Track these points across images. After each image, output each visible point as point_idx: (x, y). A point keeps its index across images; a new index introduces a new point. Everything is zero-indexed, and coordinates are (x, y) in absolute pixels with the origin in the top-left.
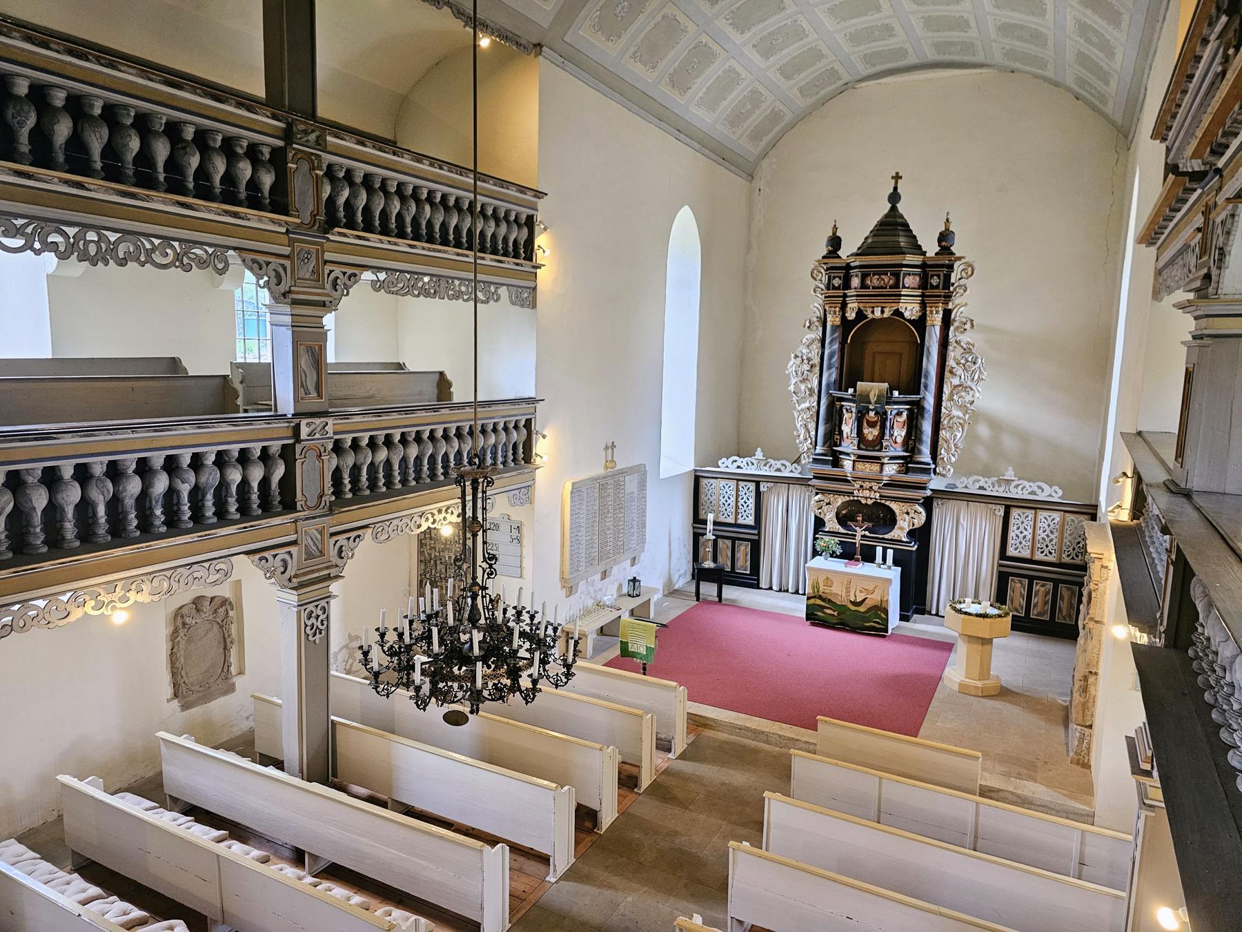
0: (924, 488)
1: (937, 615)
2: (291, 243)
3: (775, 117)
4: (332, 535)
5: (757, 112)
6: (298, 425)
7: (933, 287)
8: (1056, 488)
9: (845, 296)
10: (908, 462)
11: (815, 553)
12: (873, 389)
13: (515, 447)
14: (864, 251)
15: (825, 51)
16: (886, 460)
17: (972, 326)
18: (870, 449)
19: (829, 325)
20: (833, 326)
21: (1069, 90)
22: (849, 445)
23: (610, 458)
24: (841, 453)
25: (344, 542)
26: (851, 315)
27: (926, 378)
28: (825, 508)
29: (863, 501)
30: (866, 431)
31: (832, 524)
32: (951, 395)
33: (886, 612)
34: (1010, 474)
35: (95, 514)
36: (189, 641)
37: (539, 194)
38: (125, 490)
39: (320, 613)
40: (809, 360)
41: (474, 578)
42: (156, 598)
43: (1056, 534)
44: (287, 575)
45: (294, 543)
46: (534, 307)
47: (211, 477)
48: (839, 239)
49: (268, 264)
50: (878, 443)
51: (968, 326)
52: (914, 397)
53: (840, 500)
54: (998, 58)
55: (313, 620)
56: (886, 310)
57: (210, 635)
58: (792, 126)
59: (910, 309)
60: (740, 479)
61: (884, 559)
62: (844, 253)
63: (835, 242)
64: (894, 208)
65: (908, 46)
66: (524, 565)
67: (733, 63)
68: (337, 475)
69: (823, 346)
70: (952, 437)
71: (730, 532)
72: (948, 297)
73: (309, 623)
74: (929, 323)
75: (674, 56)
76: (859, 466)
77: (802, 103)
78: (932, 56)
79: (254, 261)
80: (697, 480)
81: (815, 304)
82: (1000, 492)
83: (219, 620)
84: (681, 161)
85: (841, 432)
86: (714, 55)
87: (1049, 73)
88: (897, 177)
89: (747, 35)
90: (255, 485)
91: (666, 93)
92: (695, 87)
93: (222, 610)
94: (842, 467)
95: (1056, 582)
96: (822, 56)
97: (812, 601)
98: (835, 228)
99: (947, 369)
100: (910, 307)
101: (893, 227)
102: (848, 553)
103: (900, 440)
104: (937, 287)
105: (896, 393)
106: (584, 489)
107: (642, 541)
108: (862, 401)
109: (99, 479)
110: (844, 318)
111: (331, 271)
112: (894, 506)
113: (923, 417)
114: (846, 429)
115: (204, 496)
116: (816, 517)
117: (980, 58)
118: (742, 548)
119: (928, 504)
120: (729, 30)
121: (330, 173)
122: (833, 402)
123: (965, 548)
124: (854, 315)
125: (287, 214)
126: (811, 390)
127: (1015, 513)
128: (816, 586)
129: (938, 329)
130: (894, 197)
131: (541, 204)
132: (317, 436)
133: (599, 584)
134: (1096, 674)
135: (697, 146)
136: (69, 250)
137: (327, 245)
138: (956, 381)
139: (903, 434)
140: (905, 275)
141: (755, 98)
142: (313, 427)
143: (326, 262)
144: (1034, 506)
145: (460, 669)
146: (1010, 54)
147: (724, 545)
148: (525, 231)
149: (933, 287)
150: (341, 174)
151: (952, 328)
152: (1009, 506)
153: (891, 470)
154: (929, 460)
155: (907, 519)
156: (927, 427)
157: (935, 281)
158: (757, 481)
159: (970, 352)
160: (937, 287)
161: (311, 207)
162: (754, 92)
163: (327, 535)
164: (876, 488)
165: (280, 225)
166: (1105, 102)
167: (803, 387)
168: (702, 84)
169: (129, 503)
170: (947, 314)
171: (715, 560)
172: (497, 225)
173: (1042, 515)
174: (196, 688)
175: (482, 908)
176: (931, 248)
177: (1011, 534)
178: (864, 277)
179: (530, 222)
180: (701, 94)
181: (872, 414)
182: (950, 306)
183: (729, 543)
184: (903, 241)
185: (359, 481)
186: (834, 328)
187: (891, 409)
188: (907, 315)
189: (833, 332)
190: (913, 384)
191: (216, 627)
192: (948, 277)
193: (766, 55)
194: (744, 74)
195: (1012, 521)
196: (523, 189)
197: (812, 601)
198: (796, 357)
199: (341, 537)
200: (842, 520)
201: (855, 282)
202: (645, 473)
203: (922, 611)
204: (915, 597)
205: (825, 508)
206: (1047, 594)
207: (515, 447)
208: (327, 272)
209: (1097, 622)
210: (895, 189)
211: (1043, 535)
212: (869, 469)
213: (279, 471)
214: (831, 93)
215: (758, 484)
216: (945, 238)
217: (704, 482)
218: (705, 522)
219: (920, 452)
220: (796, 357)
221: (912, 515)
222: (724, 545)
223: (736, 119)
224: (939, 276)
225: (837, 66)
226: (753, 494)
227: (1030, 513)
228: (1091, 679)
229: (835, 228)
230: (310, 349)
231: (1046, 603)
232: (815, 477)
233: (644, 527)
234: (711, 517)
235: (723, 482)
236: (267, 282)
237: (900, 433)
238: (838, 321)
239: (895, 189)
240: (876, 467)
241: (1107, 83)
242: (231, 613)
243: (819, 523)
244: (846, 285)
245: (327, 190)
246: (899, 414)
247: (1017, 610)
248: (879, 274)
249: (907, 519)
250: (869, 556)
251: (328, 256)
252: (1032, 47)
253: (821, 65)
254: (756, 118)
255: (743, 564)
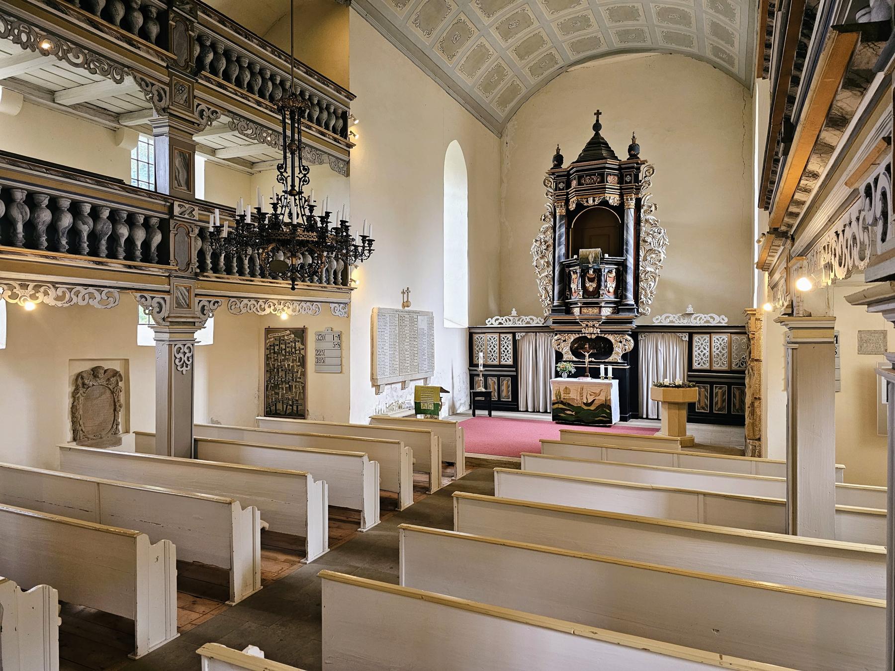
0: (631, 323)
1: (647, 418)
2: (170, 75)
3: (513, 90)
4: (196, 295)
5: (502, 83)
6: (172, 204)
7: (627, 183)
8: (723, 316)
9: (568, 194)
10: (619, 305)
11: (558, 375)
12: (591, 253)
13: (335, 273)
14: (581, 159)
15: (545, 38)
16: (603, 304)
17: (656, 208)
18: (592, 297)
19: (558, 214)
20: (560, 216)
21: (709, 61)
22: (577, 296)
23: (405, 295)
24: (572, 304)
25: (206, 304)
26: (572, 207)
27: (627, 244)
28: (562, 344)
29: (589, 337)
30: (587, 285)
31: (568, 355)
32: (645, 257)
33: (610, 408)
34: (690, 310)
35: (15, 229)
36: (87, 398)
37: (351, 96)
38: (38, 217)
39: (187, 351)
40: (546, 242)
41: (293, 186)
42: (59, 304)
43: (726, 350)
44: (162, 315)
45: (168, 292)
46: (348, 175)
47: (106, 227)
48: (561, 157)
49: (153, 85)
50: (596, 293)
51: (653, 208)
52: (619, 259)
53: (573, 337)
54: (661, 43)
55: (181, 355)
56: (597, 199)
57: (104, 397)
58: (526, 98)
59: (613, 199)
60: (501, 331)
61: (606, 373)
62: (565, 165)
63: (559, 159)
64: (597, 134)
65: (600, 35)
66: (343, 355)
67: (483, 40)
68: (201, 254)
69: (555, 232)
70: (649, 286)
71: (496, 371)
72: (638, 189)
73: (178, 356)
74: (626, 207)
75: (443, 27)
76: (585, 310)
77: (533, 81)
78: (618, 45)
79: (142, 80)
80: (471, 335)
81: (547, 204)
82: (685, 322)
83: (111, 387)
84: (452, 112)
85: (570, 289)
86: (471, 32)
87: (694, 50)
88: (598, 113)
89: (492, 19)
90: (139, 243)
91: (437, 55)
92: (458, 55)
93: (113, 380)
94: (573, 313)
95: (729, 385)
96: (543, 42)
97: (556, 406)
98: (558, 150)
99: (641, 239)
100: (612, 196)
101: (597, 147)
102: (580, 372)
103: (612, 290)
104: (630, 182)
105: (607, 256)
106: (387, 315)
107: (432, 367)
108: (584, 263)
109: (19, 203)
110: (568, 210)
111: (199, 105)
112: (610, 337)
113: (626, 272)
114: (573, 286)
115: (100, 241)
116: (556, 351)
117: (648, 44)
118: (505, 382)
119: (635, 335)
120: (479, 13)
121: (200, 39)
122: (563, 267)
123: (662, 363)
124: (574, 205)
125: (167, 50)
126: (548, 262)
127: (696, 338)
128: (558, 395)
129: (632, 211)
130: (597, 127)
131: (352, 104)
132: (186, 216)
133: (400, 392)
134: (759, 399)
135: (462, 102)
136: (7, 32)
137: (196, 85)
138: (648, 248)
139: (614, 286)
140: (608, 174)
141: (499, 71)
142: (183, 209)
143: (195, 97)
144: (707, 330)
145: (289, 365)
146: (668, 37)
147: (492, 381)
148: (341, 122)
149: (627, 183)
150: (208, 43)
151: (642, 211)
152: (692, 331)
153: (606, 312)
154: (633, 302)
155: (621, 346)
156: (630, 279)
157: (628, 179)
158: (513, 331)
159: (656, 226)
160: (630, 182)
161: (185, 56)
162: (499, 66)
163: (193, 295)
164: (597, 325)
165: (163, 60)
166: (732, 64)
167: (542, 262)
168: (464, 52)
169: (42, 228)
170: (638, 201)
171: (486, 388)
172: (321, 112)
173: (715, 337)
174: (91, 436)
175: (306, 525)
176: (623, 155)
177: (695, 353)
178: (580, 178)
179: (344, 116)
180: (462, 62)
181: (591, 272)
182: (640, 196)
183: (495, 379)
184: (604, 153)
185: (218, 265)
186: (562, 217)
187: (605, 268)
188: (611, 202)
189: (561, 220)
190: (619, 249)
191: (108, 392)
192: (637, 176)
193: (506, 36)
194: (491, 50)
195: (695, 344)
196: (339, 89)
197: (556, 406)
198: (536, 241)
199: (204, 299)
200: (574, 352)
201: (574, 183)
202: (432, 318)
203: (637, 416)
204: (631, 405)
205: (562, 344)
206: (723, 394)
207: (335, 273)
208: (195, 104)
209: (757, 360)
210: (597, 121)
211: (717, 352)
212: (591, 311)
213: (157, 238)
214: (553, 73)
215: (514, 334)
216: (633, 149)
217: (476, 337)
218: (477, 366)
219: (626, 297)
220: (536, 241)
221: (624, 343)
222: (492, 381)
223: (488, 86)
224: (630, 175)
225: (554, 52)
226: (511, 342)
227: (707, 337)
228: (756, 404)
229: (558, 150)
230: (182, 154)
231: (723, 401)
232: (554, 323)
233: (433, 357)
234: (481, 362)
235: (489, 336)
236: (152, 98)
237: (611, 285)
238: (564, 212)
239: (597, 121)
240: (596, 311)
241: (732, 45)
242: (120, 384)
243: (559, 357)
244: (568, 186)
245: (197, 50)
246: (610, 272)
247: (703, 408)
248: (590, 175)
249: (621, 346)
250: (595, 374)
251: (197, 93)
252: (682, 27)
253: (542, 52)
254: (502, 86)
255: (506, 395)
